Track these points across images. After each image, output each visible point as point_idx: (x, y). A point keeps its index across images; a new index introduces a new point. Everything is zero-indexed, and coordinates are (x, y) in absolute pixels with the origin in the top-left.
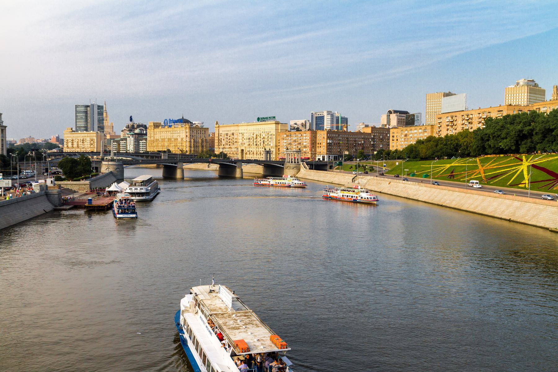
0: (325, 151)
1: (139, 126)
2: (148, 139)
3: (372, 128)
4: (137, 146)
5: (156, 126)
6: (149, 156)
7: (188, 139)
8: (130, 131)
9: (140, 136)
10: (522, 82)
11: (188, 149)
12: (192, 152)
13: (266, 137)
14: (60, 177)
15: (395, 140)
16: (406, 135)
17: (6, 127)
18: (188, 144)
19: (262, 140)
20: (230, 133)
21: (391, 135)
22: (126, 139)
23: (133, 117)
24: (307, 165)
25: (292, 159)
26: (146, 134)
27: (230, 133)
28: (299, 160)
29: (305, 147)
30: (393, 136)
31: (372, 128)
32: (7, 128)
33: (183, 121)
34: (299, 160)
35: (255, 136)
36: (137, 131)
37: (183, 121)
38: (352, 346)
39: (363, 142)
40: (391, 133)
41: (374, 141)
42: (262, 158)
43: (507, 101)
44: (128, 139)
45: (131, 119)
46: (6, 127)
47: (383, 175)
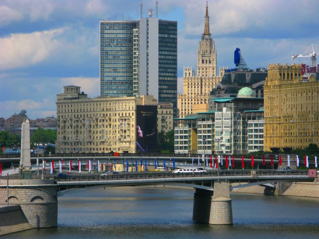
23: (242, 53)
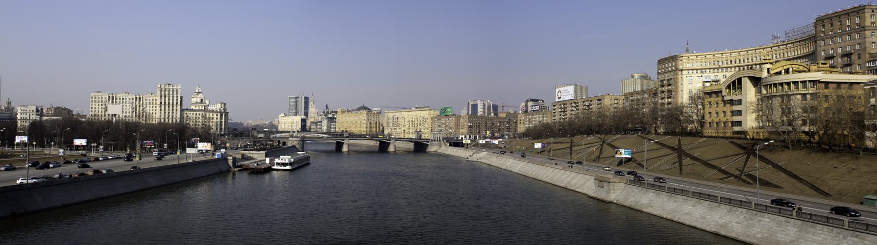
0: (466, 131)
1: (332, 112)
2: (337, 121)
3: (507, 113)
4: (329, 127)
5: (343, 112)
6: (338, 135)
7: (365, 122)
8: (326, 115)
9: (332, 120)
10: (636, 76)
11: (365, 129)
12: (368, 132)
13: (421, 120)
14: (101, 138)
15: (522, 123)
16: (530, 119)
17: (228, 113)
18: (365, 125)
19: (419, 123)
20: (395, 117)
21: (519, 119)
22: (321, 122)
23: (328, 106)
24: (447, 142)
25: (437, 138)
26: (336, 118)
27: (395, 117)
28: (441, 139)
29: (451, 128)
30: (521, 120)
31: (507, 113)
32: (229, 114)
33: (364, 108)
34: (441, 139)
35: (413, 120)
36: (330, 116)
37: (364, 108)
38: (46, 166)
39: (499, 125)
40: (519, 117)
41: (508, 124)
42: (414, 136)
43: (623, 91)
44: (323, 121)
45: (327, 107)
46: (228, 113)
47: (512, 152)
